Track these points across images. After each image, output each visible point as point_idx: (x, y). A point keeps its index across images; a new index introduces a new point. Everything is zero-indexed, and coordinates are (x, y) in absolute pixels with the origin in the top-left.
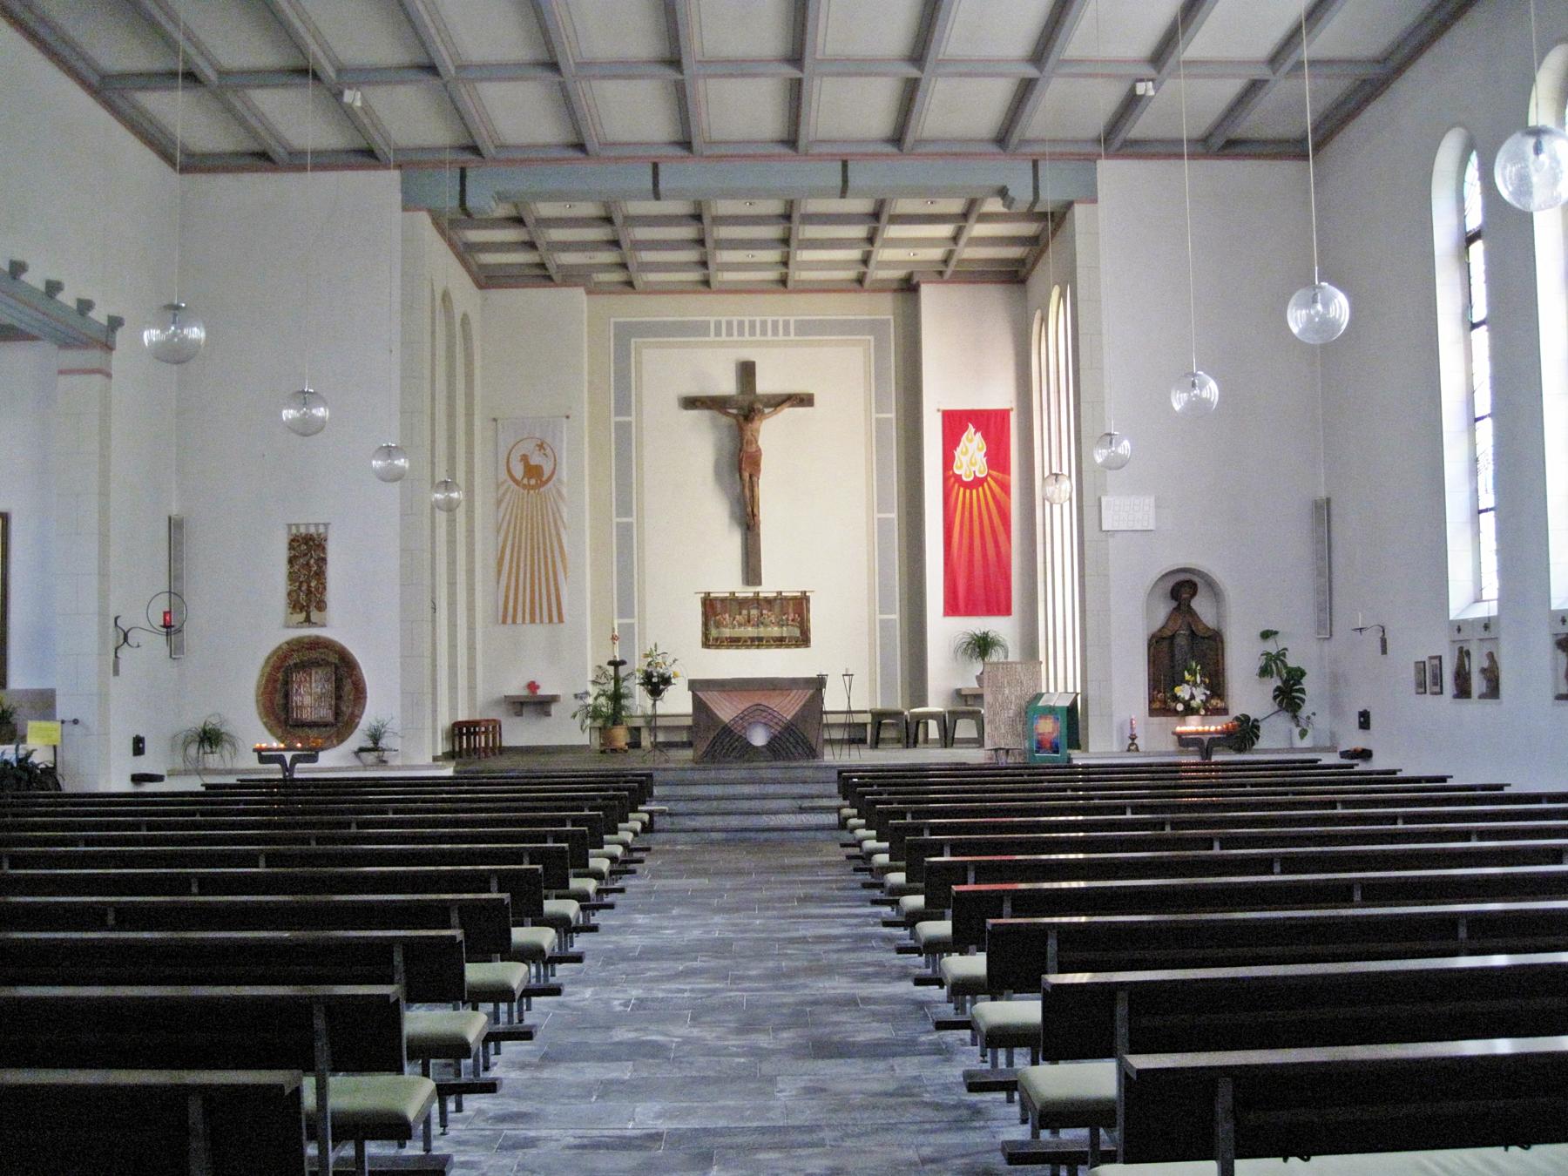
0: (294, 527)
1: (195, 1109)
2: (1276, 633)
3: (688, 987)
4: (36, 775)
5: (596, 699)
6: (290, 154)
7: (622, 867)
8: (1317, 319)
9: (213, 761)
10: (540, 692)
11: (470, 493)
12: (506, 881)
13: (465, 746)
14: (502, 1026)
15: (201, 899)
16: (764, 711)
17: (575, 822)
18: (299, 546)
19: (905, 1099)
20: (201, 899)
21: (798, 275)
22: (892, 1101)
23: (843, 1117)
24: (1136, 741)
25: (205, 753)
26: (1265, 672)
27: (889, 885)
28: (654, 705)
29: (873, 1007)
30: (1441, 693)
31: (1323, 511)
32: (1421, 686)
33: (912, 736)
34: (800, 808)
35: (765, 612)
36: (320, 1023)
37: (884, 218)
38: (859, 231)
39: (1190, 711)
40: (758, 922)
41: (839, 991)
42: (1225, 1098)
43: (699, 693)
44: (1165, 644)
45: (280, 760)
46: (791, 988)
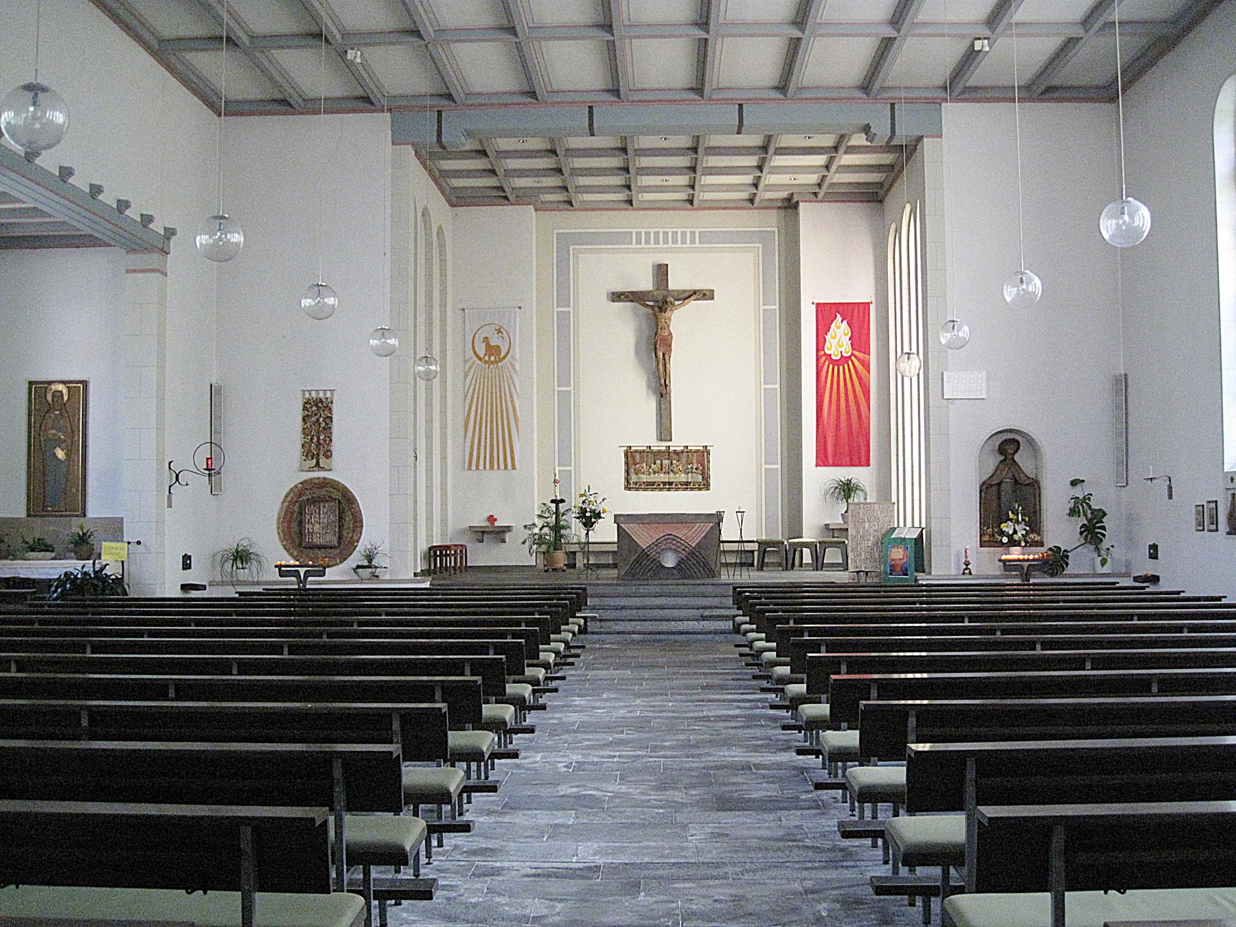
0: (307, 393)
1: (246, 833)
2: (1083, 481)
3: (617, 754)
4: (109, 583)
5: (541, 529)
6: (304, 100)
7: (564, 660)
8: (1124, 228)
9: (243, 574)
10: (496, 524)
11: (444, 366)
12: (476, 668)
13: (438, 565)
14: (473, 781)
15: (238, 677)
16: (674, 540)
17: (528, 623)
18: (311, 407)
19: (790, 843)
20: (238, 677)
21: (701, 196)
22: (781, 844)
23: (741, 857)
24: (969, 567)
25: (238, 568)
26: (1073, 512)
27: (775, 676)
28: (587, 534)
29: (763, 772)
30: (1217, 530)
31: (1122, 385)
32: (1200, 526)
33: (790, 562)
34: (702, 616)
35: (674, 462)
36: (338, 773)
37: (771, 150)
38: (752, 161)
39: (1013, 543)
40: (670, 704)
41: (736, 759)
42: (1058, 841)
43: (622, 525)
44: (994, 488)
45: (297, 574)
46: (698, 756)
